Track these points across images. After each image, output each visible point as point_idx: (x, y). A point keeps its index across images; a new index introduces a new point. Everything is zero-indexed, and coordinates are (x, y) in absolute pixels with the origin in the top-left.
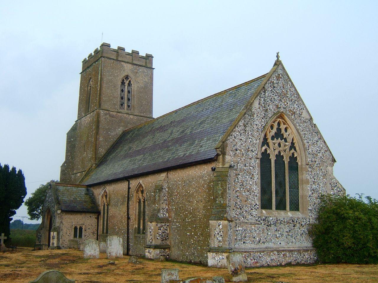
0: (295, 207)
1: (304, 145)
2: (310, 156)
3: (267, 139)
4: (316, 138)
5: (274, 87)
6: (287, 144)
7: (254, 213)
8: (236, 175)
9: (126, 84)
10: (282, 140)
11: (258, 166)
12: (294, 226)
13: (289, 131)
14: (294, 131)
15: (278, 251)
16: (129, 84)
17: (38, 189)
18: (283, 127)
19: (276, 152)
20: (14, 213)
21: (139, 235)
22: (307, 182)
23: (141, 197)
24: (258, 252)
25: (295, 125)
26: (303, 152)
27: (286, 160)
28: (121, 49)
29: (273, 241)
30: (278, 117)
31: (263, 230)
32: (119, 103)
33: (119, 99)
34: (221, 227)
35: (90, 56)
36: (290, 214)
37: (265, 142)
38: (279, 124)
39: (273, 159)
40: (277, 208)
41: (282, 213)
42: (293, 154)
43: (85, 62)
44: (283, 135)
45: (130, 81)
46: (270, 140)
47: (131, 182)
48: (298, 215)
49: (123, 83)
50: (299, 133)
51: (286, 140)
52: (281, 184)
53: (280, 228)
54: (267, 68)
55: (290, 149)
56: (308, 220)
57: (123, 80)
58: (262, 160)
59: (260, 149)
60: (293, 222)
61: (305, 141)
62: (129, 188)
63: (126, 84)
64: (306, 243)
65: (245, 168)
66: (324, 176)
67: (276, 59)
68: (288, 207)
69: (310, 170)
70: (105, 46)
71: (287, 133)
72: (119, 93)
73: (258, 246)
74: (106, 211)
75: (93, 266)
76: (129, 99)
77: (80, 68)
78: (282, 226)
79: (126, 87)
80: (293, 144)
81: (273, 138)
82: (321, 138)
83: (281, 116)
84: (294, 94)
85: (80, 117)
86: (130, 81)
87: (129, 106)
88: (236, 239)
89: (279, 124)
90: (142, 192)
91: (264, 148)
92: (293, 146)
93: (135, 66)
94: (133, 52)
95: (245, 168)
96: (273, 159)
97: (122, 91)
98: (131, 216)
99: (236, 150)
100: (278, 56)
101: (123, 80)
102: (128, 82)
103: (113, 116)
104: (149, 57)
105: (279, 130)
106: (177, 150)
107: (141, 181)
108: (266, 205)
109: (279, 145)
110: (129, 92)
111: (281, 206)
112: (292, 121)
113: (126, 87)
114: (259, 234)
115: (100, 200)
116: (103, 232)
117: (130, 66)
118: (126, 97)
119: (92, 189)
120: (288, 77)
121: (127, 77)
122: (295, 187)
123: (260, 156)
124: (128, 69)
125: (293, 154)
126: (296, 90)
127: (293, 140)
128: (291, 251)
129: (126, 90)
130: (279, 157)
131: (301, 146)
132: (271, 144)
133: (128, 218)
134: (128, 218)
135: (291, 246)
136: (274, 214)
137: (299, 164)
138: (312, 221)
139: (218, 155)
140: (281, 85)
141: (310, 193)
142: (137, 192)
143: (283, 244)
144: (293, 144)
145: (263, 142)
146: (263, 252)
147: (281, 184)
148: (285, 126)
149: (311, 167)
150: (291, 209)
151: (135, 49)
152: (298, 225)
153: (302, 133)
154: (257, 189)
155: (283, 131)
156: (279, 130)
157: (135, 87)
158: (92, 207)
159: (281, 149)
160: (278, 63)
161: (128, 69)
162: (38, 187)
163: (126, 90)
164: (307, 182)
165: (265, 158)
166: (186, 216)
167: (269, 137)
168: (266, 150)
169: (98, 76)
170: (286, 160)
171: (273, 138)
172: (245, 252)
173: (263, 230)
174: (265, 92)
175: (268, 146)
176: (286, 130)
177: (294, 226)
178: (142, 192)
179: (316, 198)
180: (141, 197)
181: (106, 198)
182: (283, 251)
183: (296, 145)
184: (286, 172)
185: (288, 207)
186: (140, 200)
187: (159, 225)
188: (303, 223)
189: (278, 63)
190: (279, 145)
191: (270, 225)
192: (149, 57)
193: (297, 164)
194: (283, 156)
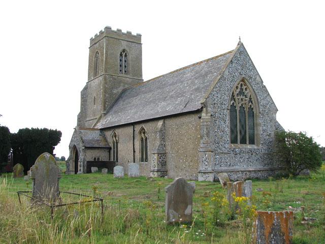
0: (252, 142)
1: (257, 99)
2: (262, 107)
3: (234, 96)
4: (265, 95)
6: (247, 99)
7: (227, 146)
9: (124, 56)
12: (252, 155)
13: (248, 89)
15: (242, 171)
16: (126, 56)
18: (244, 87)
19: (240, 105)
21: (142, 163)
23: (143, 136)
25: (251, 86)
26: (257, 104)
27: (246, 110)
29: (239, 164)
33: (119, 66)
34: (207, 155)
35: (96, 36)
36: (249, 147)
37: (233, 98)
41: (244, 146)
42: (251, 106)
43: (92, 40)
45: (126, 54)
46: (236, 97)
47: (135, 126)
48: (255, 147)
49: (121, 55)
50: (254, 92)
54: (233, 46)
55: (231, 100)
57: (121, 53)
60: (251, 152)
61: (259, 97)
62: (134, 131)
63: (124, 56)
67: (239, 40)
68: (248, 142)
70: (108, 29)
71: (247, 92)
74: (115, 147)
75: (304, 188)
76: (125, 67)
77: (88, 44)
78: (244, 155)
80: (250, 99)
82: (269, 94)
85: (90, 81)
87: (125, 71)
89: (241, 85)
90: (144, 133)
91: (232, 102)
92: (250, 101)
94: (118, 30)
96: (238, 109)
97: (121, 60)
100: (240, 39)
103: (115, 79)
104: (139, 36)
107: (143, 125)
108: (234, 141)
111: (243, 141)
115: (110, 140)
116: (114, 160)
117: (125, 42)
119: (104, 131)
121: (124, 51)
123: (229, 108)
125: (251, 106)
126: (252, 62)
128: (250, 171)
129: (124, 60)
131: (256, 101)
132: (236, 100)
133: (134, 152)
134: (134, 152)
136: (239, 147)
137: (255, 113)
139: (202, 108)
142: (140, 133)
144: (250, 99)
146: (233, 172)
147: (243, 127)
148: (245, 87)
149: (263, 115)
150: (241, 143)
151: (120, 28)
152: (254, 154)
153: (256, 92)
154: (228, 130)
155: (244, 90)
157: (130, 57)
158: (106, 145)
159: (243, 102)
160: (241, 45)
161: (124, 45)
163: (124, 60)
165: (233, 109)
167: (235, 94)
168: (233, 103)
169: (103, 51)
170: (246, 110)
171: (237, 96)
174: (232, 64)
175: (235, 101)
176: (246, 89)
177: (252, 155)
178: (144, 133)
180: (143, 136)
181: (115, 137)
182: (245, 171)
185: (248, 142)
186: (142, 138)
189: (241, 45)
192: (139, 36)
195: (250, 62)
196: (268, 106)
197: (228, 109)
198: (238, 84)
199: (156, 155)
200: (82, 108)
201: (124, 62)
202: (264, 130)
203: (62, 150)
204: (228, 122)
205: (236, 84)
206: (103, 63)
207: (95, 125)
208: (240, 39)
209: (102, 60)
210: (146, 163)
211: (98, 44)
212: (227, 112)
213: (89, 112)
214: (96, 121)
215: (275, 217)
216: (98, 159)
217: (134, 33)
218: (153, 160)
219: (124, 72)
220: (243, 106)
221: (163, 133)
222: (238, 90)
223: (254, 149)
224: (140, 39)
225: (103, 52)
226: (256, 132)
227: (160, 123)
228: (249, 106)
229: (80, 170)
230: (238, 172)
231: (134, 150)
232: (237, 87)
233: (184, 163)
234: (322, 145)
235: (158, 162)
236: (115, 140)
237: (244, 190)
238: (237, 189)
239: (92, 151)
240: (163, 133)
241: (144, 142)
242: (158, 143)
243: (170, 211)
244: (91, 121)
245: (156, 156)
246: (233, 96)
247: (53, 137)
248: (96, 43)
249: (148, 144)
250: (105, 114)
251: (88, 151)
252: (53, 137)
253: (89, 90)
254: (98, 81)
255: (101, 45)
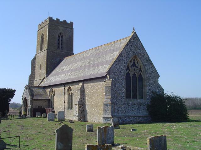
0: (142, 98)
1: (145, 69)
3: (129, 67)
4: (151, 66)
5: (132, 43)
8: (115, 83)
9: (60, 37)
10: (135, 67)
11: (101, 74)
14: (141, 63)
16: (62, 37)
17: (5, 89)
18: (136, 61)
19: (133, 73)
20: (11, 100)
22: (147, 86)
23: (70, 93)
24: (124, 117)
25: (141, 60)
27: (137, 76)
28: (58, 20)
30: (134, 57)
31: (127, 107)
32: (57, 47)
37: (128, 68)
38: (134, 60)
39: (131, 76)
40: (133, 98)
42: (140, 73)
44: (136, 65)
45: (62, 35)
46: (130, 68)
47: (65, 85)
48: (143, 101)
49: (59, 36)
51: (137, 68)
52: (135, 87)
53: (134, 107)
55: (127, 70)
56: (147, 103)
57: (59, 35)
58: (126, 76)
59: (125, 71)
60: (140, 104)
62: (64, 88)
63: (60, 37)
64: (146, 113)
65: (119, 80)
66: (154, 83)
68: (138, 98)
69: (148, 80)
72: (57, 41)
73: (124, 115)
76: (62, 44)
78: (135, 106)
79: (60, 38)
81: (131, 66)
83: (135, 57)
84: (141, 46)
86: (62, 35)
87: (62, 47)
88: (115, 112)
89: (134, 60)
91: (127, 71)
92: (140, 70)
93: (65, 28)
95: (119, 80)
96: (131, 76)
97: (59, 40)
98: (65, 102)
99: (115, 72)
100: (134, 29)
101: (59, 35)
102: (61, 36)
103: (54, 53)
105: (134, 63)
106: (87, 71)
108: (128, 96)
109: (134, 69)
110: (62, 40)
111: (135, 97)
112: (140, 58)
113: (60, 38)
114: (125, 109)
118: (60, 43)
120: (138, 38)
121: (61, 34)
122: (141, 88)
123: (125, 75)
124: (61, 28)
127: (140, 67)
128: (139, 117)
130: (134, 75)
131: (144, 70)
133: (64, 102)
134: (64, 102)
135: (139, 115)
137: (143, 78)
138: (149, 103)
140: (135, 42)
141: (148, 91)
143: (135, 113)
144: (140, 69)
145: (127, 69)
146: (127, 117)
147: (135, 87)
148: (137, 61)
149: (149, 79)
154: (124, 90)
155: (136, 63)
156: (134, 63)
157: (64, 38)
162: (11, 88)
163: (60, 40)
164: (147, 86)
165: (128, 76)
166: (92, 102)
168: (128, 72)
169: (47, 33)
170: (137, 76)
171: (131, 66)
172: (119, 117)
173: (127, 107)
174: (128, 46)
177: (141, 106)
179: (151, 93)
182: (136, 116)
183: (142, 69)
184: (137, 83)
187: (80, 106)
188: (145, 104)
190: (134, 69)
191: (130, 105)
193: (142, 78)
194: (136, 75)
195: (140, 44)
196: (153, 73)
197: (124, 76)
198: (132, 59)
199: (77, 105)
200: (32, 72)
201: (60, 41)
202: (149, 90)
203: (17, 100)
204: (124, 84)
205: (130, 59)
206: (46, 42)
207: (39, 85)
208: (134, 29)
209: (46, 40)
210: (72, 110)
211: (43, 28)
212: (124, 78)
213: (37, 74)
214: (41, 80)
215: (139, 148)
216: (41, 107)
217: (68, 22)
218: (76, 107)
219: (60, 47)
220: (135, 74)
221: (82, 91)
222: (132, 64)
223: (142, 102)
224: (72, 26)
225: (47, 34)
226: (143, 91)
227: (81, 84)
228: (139, 74)
229: (28, 114)
230: (131, 117)
231: (64, 101)
232: (131, 62)
233: (95, 111)
234: (198, 96)
235: (78, 110)
236: (52, 94)
237: (108, 131)
238: (104, 131)
239: (94, 75)
240: (82, 91)
241: (70, 96)
242: (79, 98)
243: (58, 143)
244: (38, 81)
245: (77, 106)
246: (128, 67)
247: (10, 93)
248: (42, 28)
249: (73, 98)
250: (47, 76)
251: (34, 101)
252: (10, 93)
253: (37, 60)
254: (44, 53)
255: (46, 29)
